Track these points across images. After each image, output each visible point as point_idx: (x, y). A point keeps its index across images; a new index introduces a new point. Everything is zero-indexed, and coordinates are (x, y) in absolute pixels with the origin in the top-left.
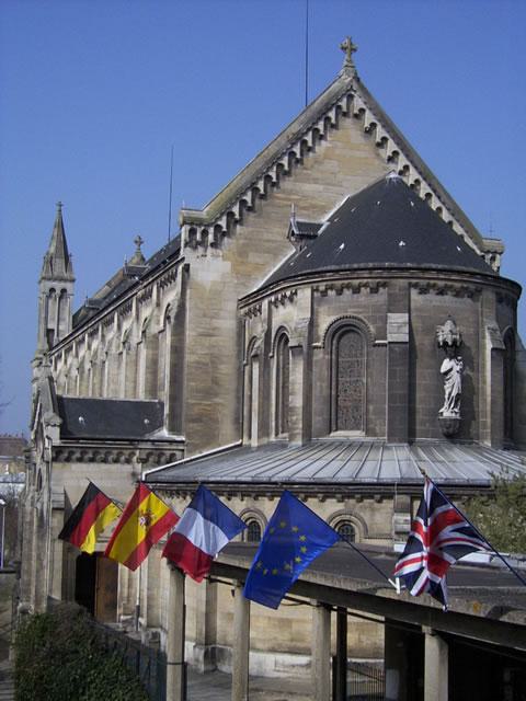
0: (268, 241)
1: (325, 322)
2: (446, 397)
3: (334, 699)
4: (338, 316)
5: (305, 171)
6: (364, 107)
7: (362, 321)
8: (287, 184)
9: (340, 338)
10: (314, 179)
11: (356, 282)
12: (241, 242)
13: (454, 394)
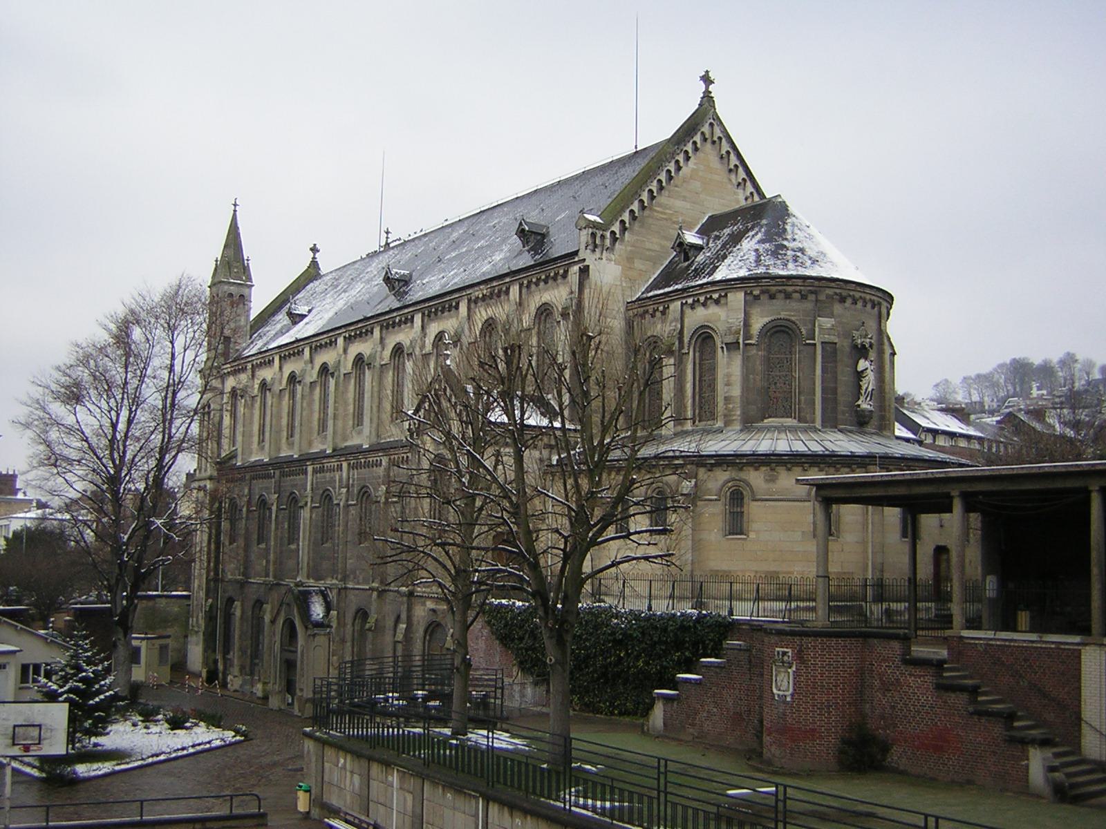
0: (649, 250)
1: (758, 323)
2: (863, 392)
3: (1102, 645)
4: (773, 318)
5: (676, 189)
6: (721, 135)
7: (794, 323)
8: (662, 199)
9: (776, 332)
10: (684, 197)
11: (790, 289)
12: (629, 248)
13: (870, 389)
